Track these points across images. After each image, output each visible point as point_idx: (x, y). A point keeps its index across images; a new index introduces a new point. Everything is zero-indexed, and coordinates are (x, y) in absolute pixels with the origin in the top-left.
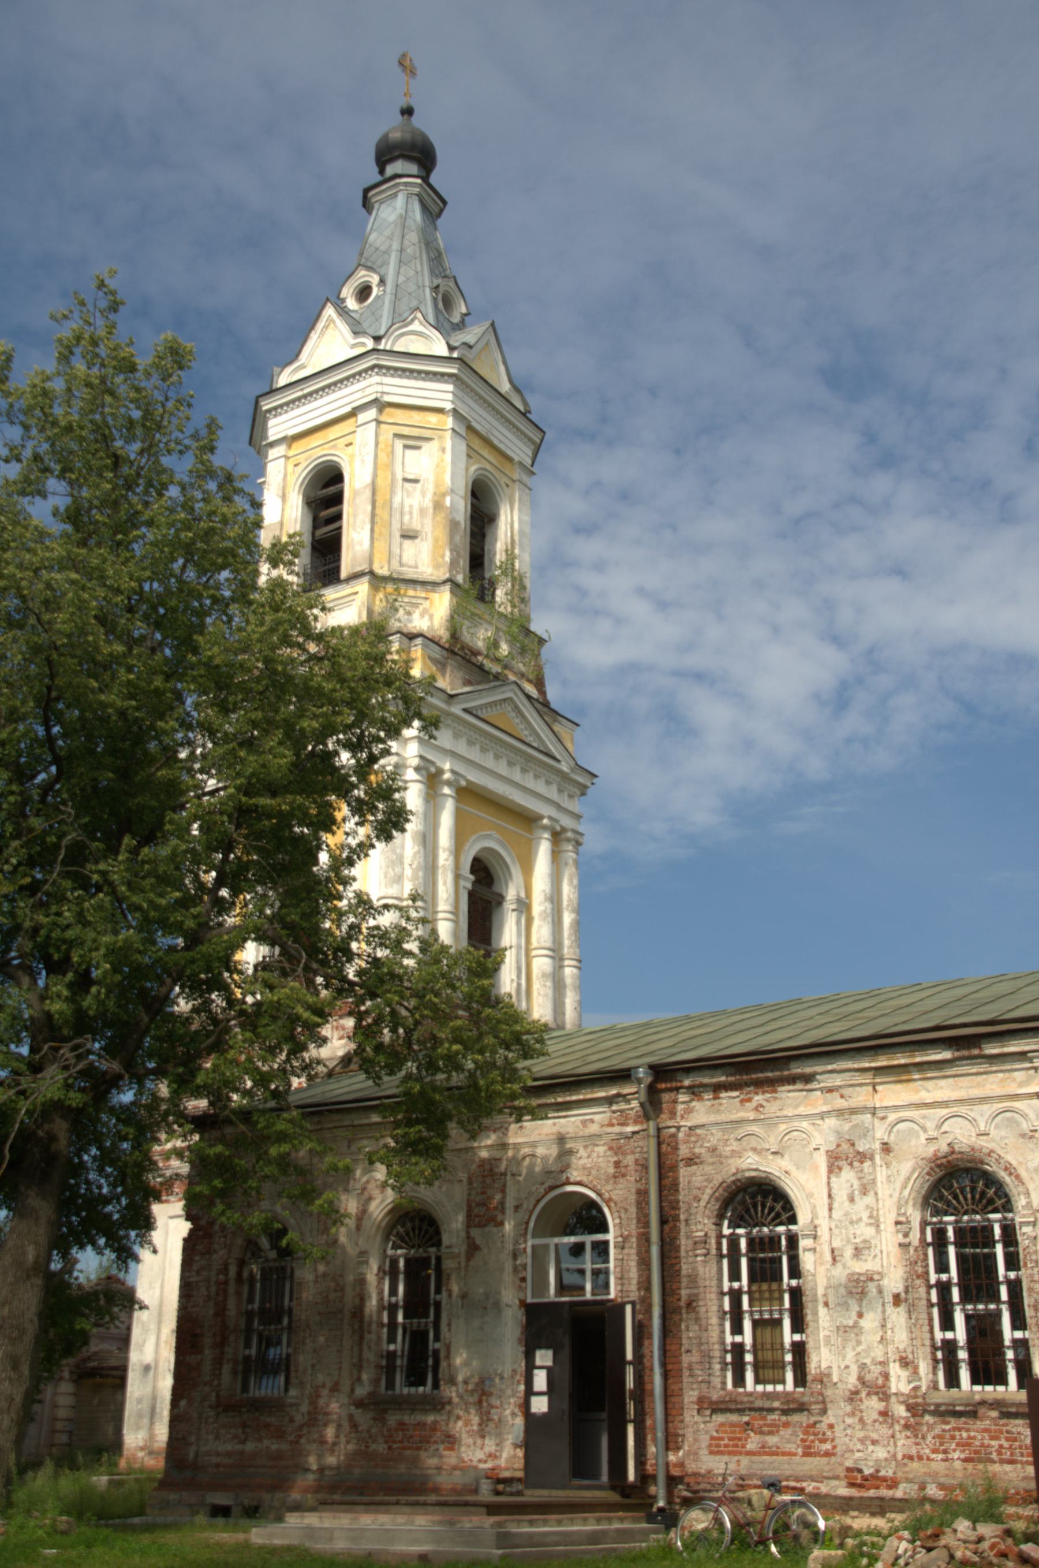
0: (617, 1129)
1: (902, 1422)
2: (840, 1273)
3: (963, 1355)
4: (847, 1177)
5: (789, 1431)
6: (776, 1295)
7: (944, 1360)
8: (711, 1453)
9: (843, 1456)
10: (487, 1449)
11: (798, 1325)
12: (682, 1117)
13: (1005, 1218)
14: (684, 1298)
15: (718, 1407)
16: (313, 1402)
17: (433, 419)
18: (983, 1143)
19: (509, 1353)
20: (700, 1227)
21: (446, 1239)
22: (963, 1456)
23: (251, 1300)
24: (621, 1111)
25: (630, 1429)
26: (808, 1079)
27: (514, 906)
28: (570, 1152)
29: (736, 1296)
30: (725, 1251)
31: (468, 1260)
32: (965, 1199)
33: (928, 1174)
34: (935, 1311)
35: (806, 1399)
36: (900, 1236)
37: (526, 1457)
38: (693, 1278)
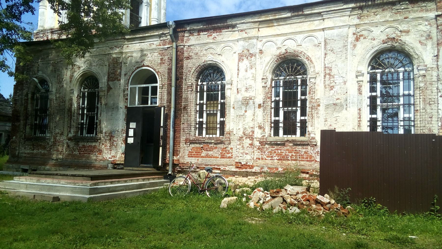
0: (162, 47)
1: (257, 147)
2: (240, 97)
3: (281, 125)
4: (246, 62)
5: (217, 150)
6: (216, 105)
7: (274, 127)
8: (189, 157)
9: (235, 158)
10: (112, 154)
11: (223, 115)
12: (186, 42)
13: (303, 77)
14: (183, 106)
15: (192, 142)
16: (55, 138)
18: (300, 49)
19: (121, 124)
20: (190, 81)
21: (100, 86)
22: (278, 158)
23: (37, 105)
24: (164, 40)
25: (161, 148)
26: (233, 26)
27: (146, 4)
28: (145, 55)
29: (201, 105)
30: (198, 90)
31: (108, 92)
32: (289, 71)
33: (276, 61)
34: (273, 110)
35: (223, 140)
36: (263, 83)
37: (125, 157)
38: (186, 99)
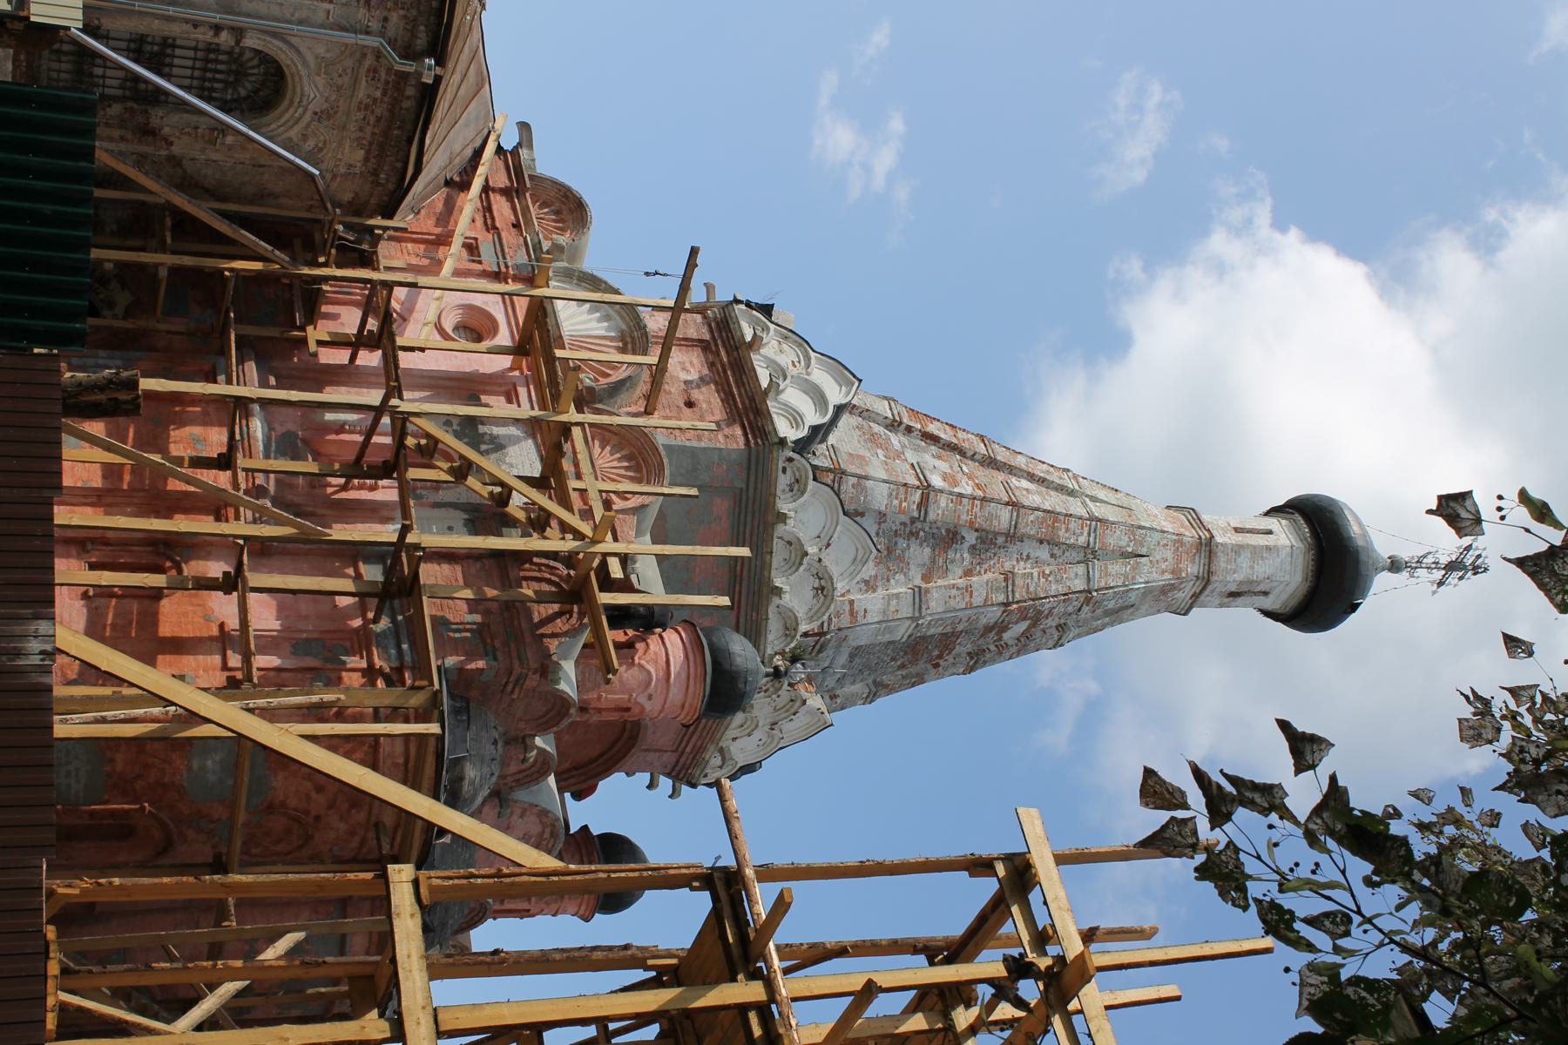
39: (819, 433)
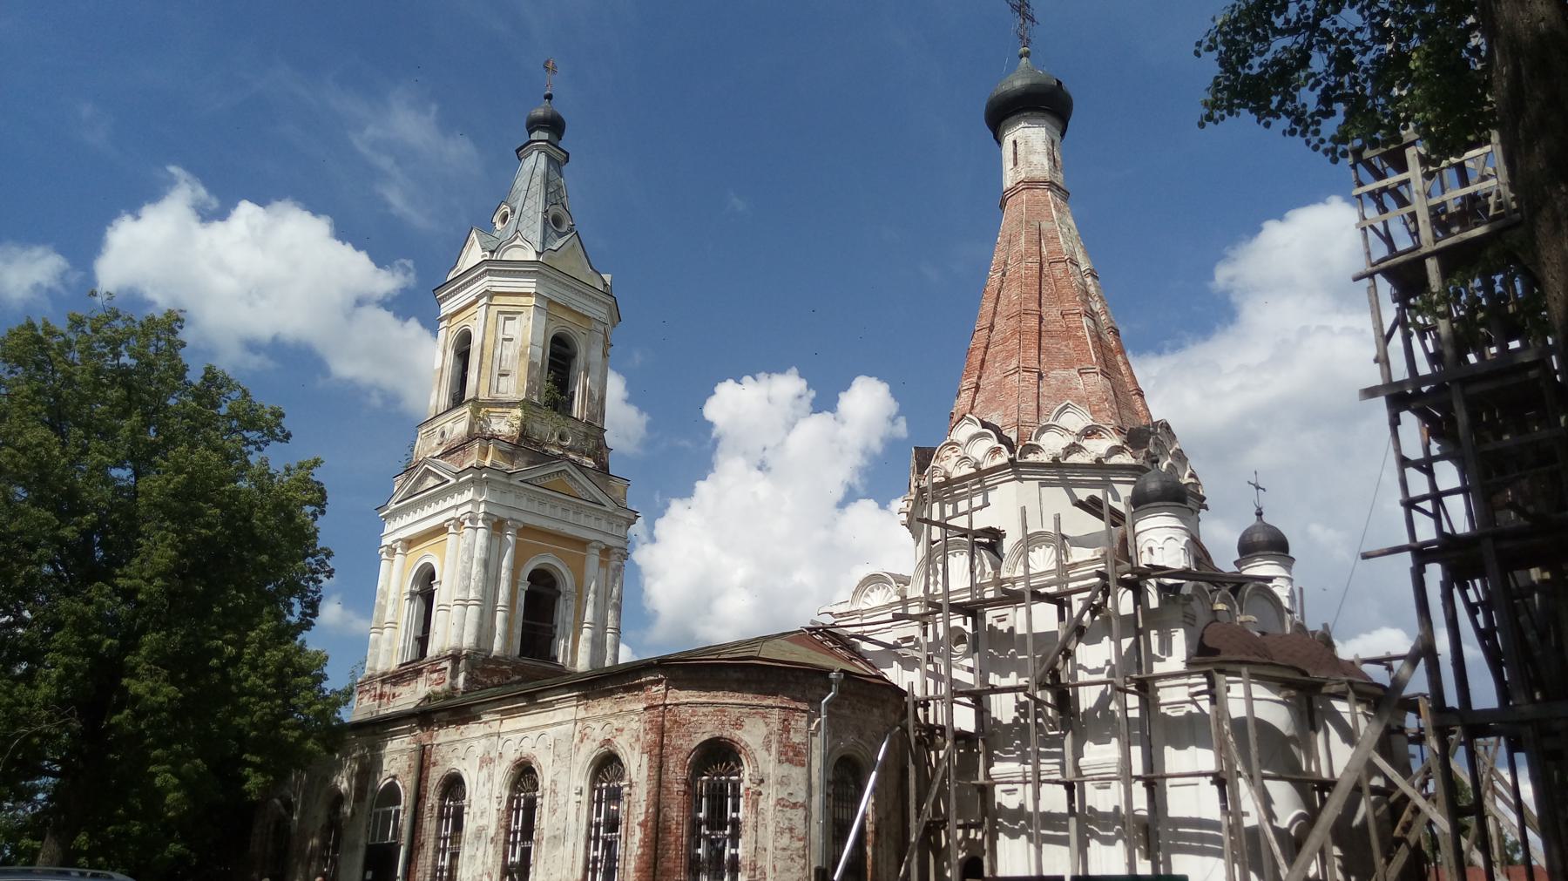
17: (523, 300)
39: (1003, 439)
